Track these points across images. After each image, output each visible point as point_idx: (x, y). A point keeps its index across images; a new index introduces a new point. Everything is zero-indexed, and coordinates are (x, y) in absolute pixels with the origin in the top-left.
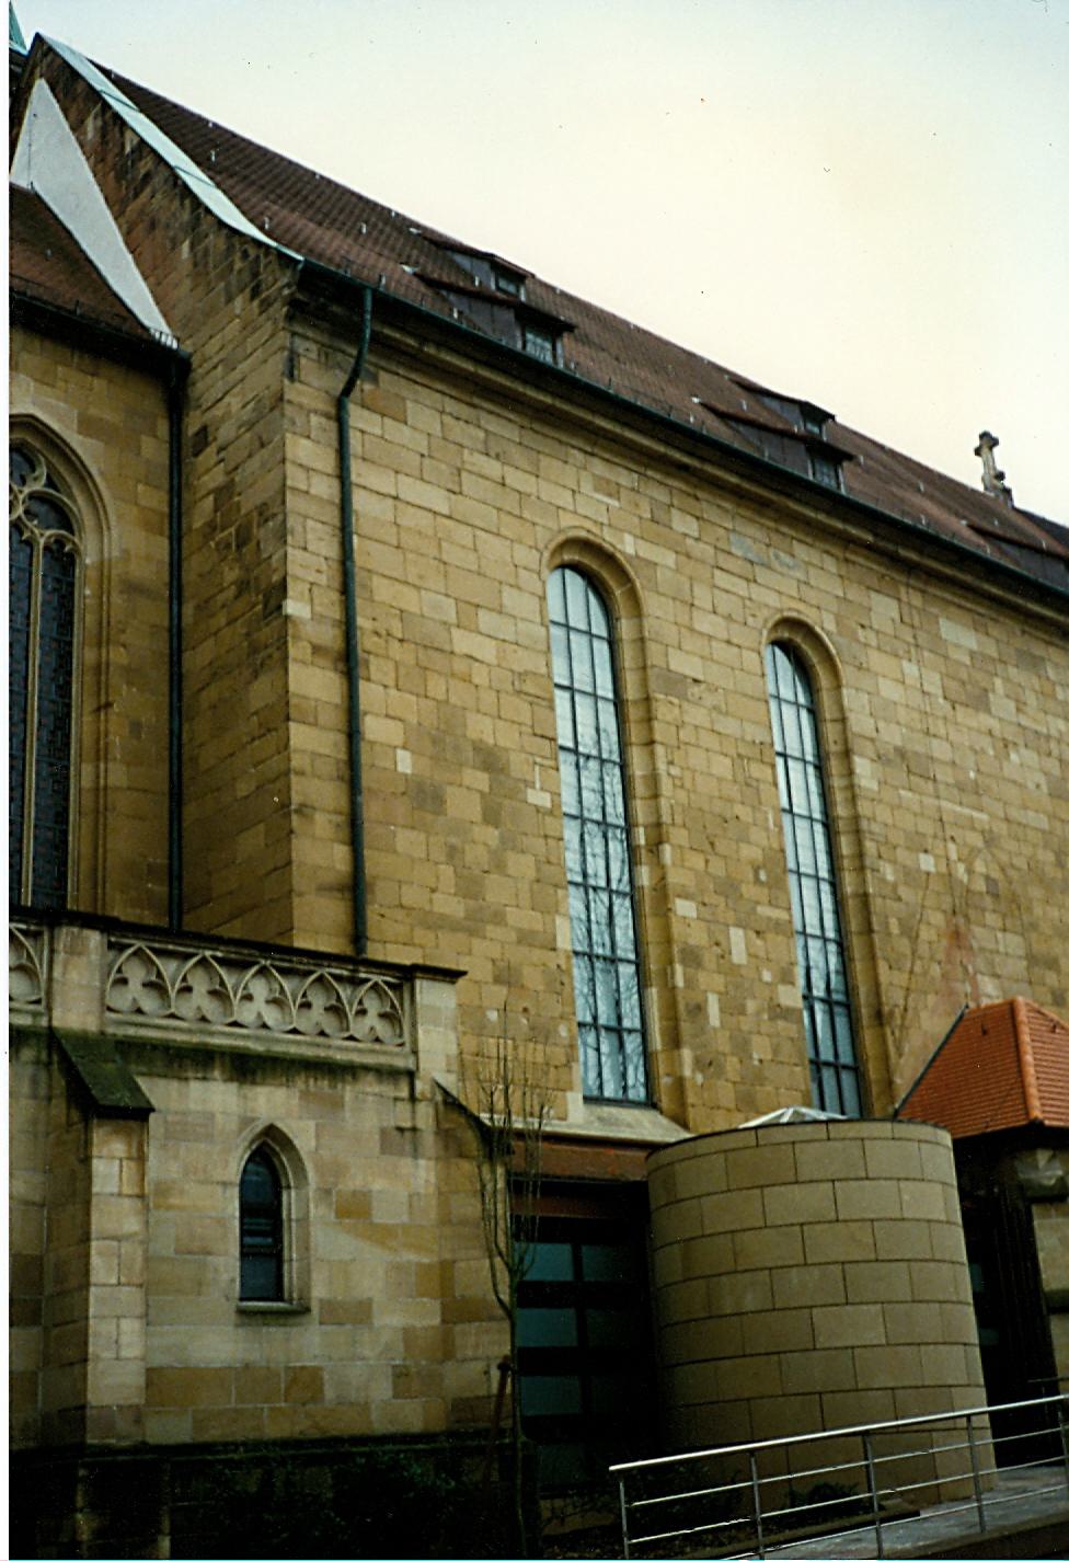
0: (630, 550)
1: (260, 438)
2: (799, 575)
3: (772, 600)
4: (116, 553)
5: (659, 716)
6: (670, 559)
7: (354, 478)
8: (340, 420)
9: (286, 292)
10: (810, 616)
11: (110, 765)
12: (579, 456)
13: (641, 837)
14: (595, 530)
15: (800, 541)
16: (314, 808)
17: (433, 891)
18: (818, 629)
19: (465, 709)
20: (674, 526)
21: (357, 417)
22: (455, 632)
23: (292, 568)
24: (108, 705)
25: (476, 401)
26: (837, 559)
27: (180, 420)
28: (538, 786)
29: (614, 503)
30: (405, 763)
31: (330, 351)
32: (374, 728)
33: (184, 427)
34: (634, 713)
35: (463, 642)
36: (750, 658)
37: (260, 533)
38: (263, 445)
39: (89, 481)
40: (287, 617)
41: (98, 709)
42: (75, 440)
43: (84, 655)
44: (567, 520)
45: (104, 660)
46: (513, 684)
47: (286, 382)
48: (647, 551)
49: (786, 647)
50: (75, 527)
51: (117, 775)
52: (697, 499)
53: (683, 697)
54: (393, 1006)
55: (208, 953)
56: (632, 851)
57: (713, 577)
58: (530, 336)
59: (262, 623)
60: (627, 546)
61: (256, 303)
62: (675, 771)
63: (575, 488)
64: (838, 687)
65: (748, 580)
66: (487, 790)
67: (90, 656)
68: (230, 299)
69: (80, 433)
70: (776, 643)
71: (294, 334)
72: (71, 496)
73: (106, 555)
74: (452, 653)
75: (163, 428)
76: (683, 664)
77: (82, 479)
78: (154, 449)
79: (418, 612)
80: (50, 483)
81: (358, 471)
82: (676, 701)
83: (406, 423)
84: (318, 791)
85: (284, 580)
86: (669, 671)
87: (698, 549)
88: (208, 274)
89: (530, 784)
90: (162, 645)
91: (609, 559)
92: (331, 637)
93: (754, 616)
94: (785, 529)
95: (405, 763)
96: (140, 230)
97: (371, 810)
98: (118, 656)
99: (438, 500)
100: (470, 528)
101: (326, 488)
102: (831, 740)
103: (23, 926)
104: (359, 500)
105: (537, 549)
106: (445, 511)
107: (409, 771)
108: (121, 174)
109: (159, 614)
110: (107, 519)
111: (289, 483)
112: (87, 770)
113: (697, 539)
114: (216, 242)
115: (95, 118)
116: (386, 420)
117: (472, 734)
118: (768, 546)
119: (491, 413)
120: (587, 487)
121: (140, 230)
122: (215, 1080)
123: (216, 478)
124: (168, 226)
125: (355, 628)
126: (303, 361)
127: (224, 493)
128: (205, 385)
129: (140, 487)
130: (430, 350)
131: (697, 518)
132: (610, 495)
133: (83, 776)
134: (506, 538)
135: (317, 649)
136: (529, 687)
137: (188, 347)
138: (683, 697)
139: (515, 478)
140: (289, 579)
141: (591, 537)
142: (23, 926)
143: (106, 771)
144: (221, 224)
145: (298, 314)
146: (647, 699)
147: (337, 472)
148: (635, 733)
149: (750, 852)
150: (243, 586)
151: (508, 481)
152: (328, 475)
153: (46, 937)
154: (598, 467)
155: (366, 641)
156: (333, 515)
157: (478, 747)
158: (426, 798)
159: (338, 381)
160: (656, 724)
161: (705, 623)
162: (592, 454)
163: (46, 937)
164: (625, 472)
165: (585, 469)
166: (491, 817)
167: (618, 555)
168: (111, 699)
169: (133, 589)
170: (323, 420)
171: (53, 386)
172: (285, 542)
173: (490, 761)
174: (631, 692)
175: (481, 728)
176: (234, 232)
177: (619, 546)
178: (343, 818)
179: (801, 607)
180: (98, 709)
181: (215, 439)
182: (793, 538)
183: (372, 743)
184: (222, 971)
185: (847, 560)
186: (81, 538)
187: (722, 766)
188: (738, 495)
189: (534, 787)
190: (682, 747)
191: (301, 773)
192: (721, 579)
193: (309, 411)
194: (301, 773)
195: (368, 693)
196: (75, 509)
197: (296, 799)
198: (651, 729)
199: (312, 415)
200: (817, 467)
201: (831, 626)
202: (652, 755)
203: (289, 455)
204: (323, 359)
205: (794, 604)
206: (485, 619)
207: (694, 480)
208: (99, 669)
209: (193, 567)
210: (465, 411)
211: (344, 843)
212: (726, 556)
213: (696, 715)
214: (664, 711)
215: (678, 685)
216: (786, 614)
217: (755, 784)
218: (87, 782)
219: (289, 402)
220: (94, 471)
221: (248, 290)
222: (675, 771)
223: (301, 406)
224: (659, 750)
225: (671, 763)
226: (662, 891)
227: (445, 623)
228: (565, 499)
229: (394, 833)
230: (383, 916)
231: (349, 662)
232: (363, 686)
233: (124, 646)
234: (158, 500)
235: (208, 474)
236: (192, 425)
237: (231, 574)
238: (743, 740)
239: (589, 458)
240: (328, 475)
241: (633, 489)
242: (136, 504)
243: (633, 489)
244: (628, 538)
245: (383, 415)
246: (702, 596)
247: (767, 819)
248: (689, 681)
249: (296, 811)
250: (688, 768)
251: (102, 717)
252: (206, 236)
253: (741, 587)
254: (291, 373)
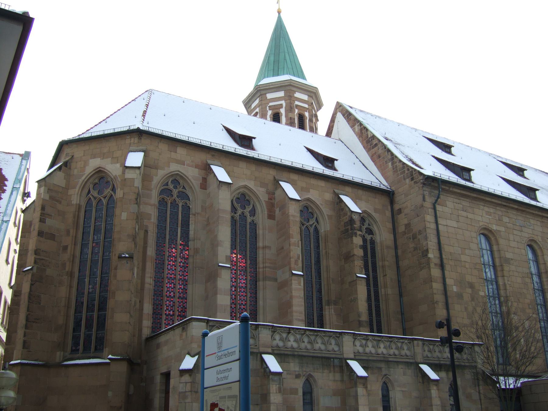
0: (495, 229)
1: (417, 214)
2: (531, 227)
3: (527, 235)
4: (384, 240)
5: (505, 269)
6: (503, 229)
7: (439, 223)
8: (435, 209)
9: (422, 181)
10: (536, 238)
11: (388, 289)
12: (482, 207)
13: (502, 299)
14: (487, 225)
15: (531, 219)
16: (439, 302)
17: (463, 318)
18: (537, 241)
19: (465, 274)
20: (504, 220)
21: (439, 208)
22: (462, 256)
23: (429, 246)
24: (386, 275)
25: (460, 198)
26: (540, 222)
27: (393, 206)
28: (481, 291)
29: (490, 217)
30: (455, 289)
31: (431, 193)
32: (449, 281)
33: (394, 208)
34: (499, 269)
35: (463, 258)
36: (523, 251)
37: (419, 237)
38: (418, 216)
39: (377, 223)
40: (429, 258)
41: (384, 276)
42: (373, 214)
43: (379, 264)
44: (481, 224)
45: (384, 265)
46: (474, 267)
47: (423, 202)
48: (499, 228)
49: (530, 246)
50: (374, 234)
51: (390, 291)
52: (508, 212)
53: (510, 264)
54: (471, 352)
55: (438, 344)
56: (500, 303)
57: (513, 232)
58: (464, 173)
59: (422, 258)
60: (494, 227)
61: (413, 182)
62: (509, 283)
63: (482, 215)
64: (543, 255)
65: (521, 231)
66: (471, 293)
67: (380, 263)
68: (405, 179)
69: (375, 213)
70: (528, 245)
71: (424, 190)
72: (373, 227)
73: (382, 240)
74: (461, 261)
75: (389, 207)
76: (509, 255)
77: (375, 223)
78: (388, 214)
79: (454, 252)
80: (369, 225)
81: (440, 221)
82: (508, 265)
83: (447, 207)
84: (439, 297)
85: (428, 249)
86: (506, 257)
87: (509, 225)
88: (397, 172)
89: (480, 290)
90: (394, 259)
91: (490, 231)
92: (438, 261)
93: (523, 240)
94: (528, 216)
95: (455, 289)
96: (375, 156)
97: (450, 301)
98: (387, 263)
99: (454, 224)
100: (462, 230)
101: (433, 226)
102: (542, 269)
103: (408, 341)
104: (441, 227)
105: (476, 232)
106: (456, 227)
107: (456, 291)
108: (368, 142)
109: (393, 252)
110: (381, 231)
111: (426, 226)
112: (383, 290)
113: (509, 223)
114: (400, 165)
115: (358, 126)
116: (443, 207)
117: (467, 280)
118: (524, 221)
119: (463, 200)
120: (484, 215)
121: (375, 156)
122: (442, 371)
123: (406, 221)
124: (384, 158)
125: (443, 258)
126: (426, 196)
127: (408, 226)
128: (399, 198)
129: (387, 223)
130: (451, 189)
131: (508, 217)
132: (489, 215)
133: (382, 291)
134: (469, 231)
135: (436, 264)
136: (477, 267)
137: (393, 188)
138: (510, 264)
139: (470, 216)
140: (429, 249)
141: (487, 227)
142: (408, 341)
143: (387, 290)
144: (400, 161)
145: (424, 186)
146: (502, 265)
147: (435, 222)
148: (499, 274)
149: (527, 301)
150: (415, 249)
151: (468, 217)
152: (433, 223)
153: (412, 343)
154: (486, 209)
155: (445, 261)
156: (435, 232)
157: (469, 283)
158: (460, 296)
159: (433, 199)
160: (504, 272)
161: (513, 244)
162: (485, 206)
163: (412, 343)
164: (492, 209)
165: (483, 210)
166: (473, 299)
167: (493, 231)
168: (386, 274)
169: (388, 247)
170: (431, 210)
171: (368, 203)
172: (427, 240)
173: (471, 286)
174: (498, 264)
175: (469, 278)
176: (404, 164)
177: (492, 228)
178: (444, 303)
179: (533, 236)
180: (384, 276)
181: (404, 212)
182: (530, 218)
183: (448, 285)
184: (440, 347)
185: (542, 222)
186: (376, 236)
187: (519, 280)
188: (517, 209)
189: (480, 291)
190: (510, 276)
191: (435, 294)
192: (515, 232)
193: (428, 208)
194: (435, 294)
195: (447, 273)
196: (374, 230)
197: (435, 300)
198: (503, 273)
199: (429, 209)
200: (530, 193)
201: (540, 240)
202: (504, 279)
203: (426, 219)
204: (429, 195)
205: (531, 236)
206: (467, 251)
207: (507, 208)
208: (383, 267)
209: (400, 242)
210: (458, 201)
211: (445, 309)
212: (515, 226)
213: (513, 268)
214: (506, 268)
215: (508, 261)
216: (530, 238)
217: (527, 283)
218: (383, 293)
219: (424, 207)
220: (378, 220)
221: (410, 178)
222: (509, 283)
223: (427, 207)
224: (506, 278)
225: (508, 281)
226: (508, 313)
227: (459, 254)
228: (480, 218)
229: (454, 305)
230: (454, 325)
231: (442, 266)
232: (446, 272)
233: (387, 261)
234: (390, 225)
235: (402, 220)
236: (396, 207)
237: (412, 245)
238: (523, 273)
239: (484, 207)
240: (433, 223)
241: (494, 213)
242: (386, 227)
243: (494, 213)
244: (494, 225)
245: (442, 206)
246: (511, 237)
247: (530, 292)
248: (510, 259)
249: (436, 303)
250: (512, 282)
251: (385, 278)
252: (396, 163)
253: (519, 233)
254: (424, 200)
